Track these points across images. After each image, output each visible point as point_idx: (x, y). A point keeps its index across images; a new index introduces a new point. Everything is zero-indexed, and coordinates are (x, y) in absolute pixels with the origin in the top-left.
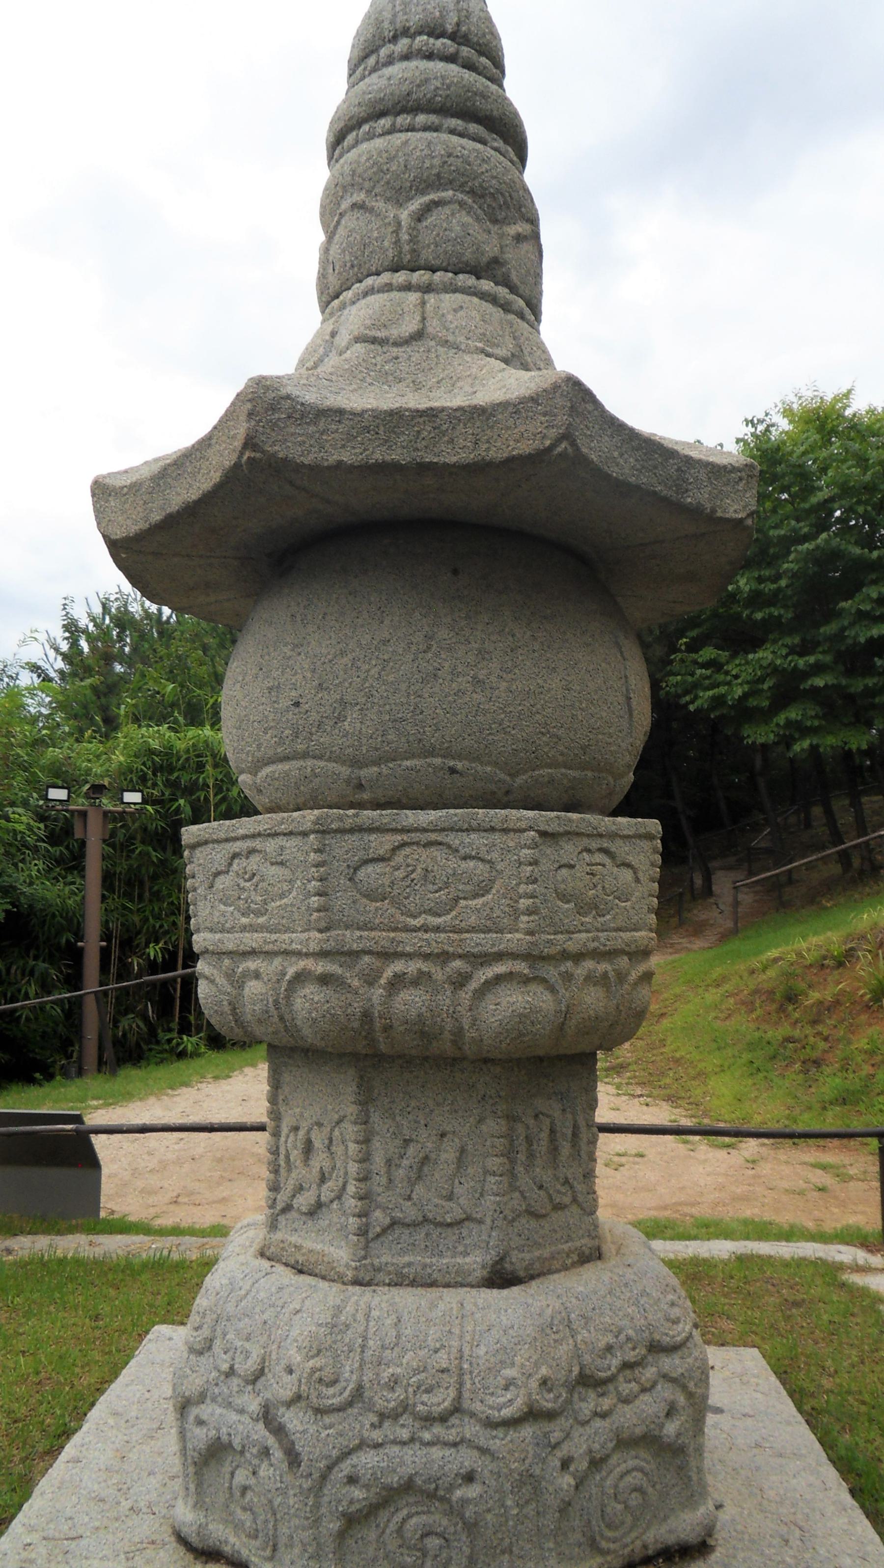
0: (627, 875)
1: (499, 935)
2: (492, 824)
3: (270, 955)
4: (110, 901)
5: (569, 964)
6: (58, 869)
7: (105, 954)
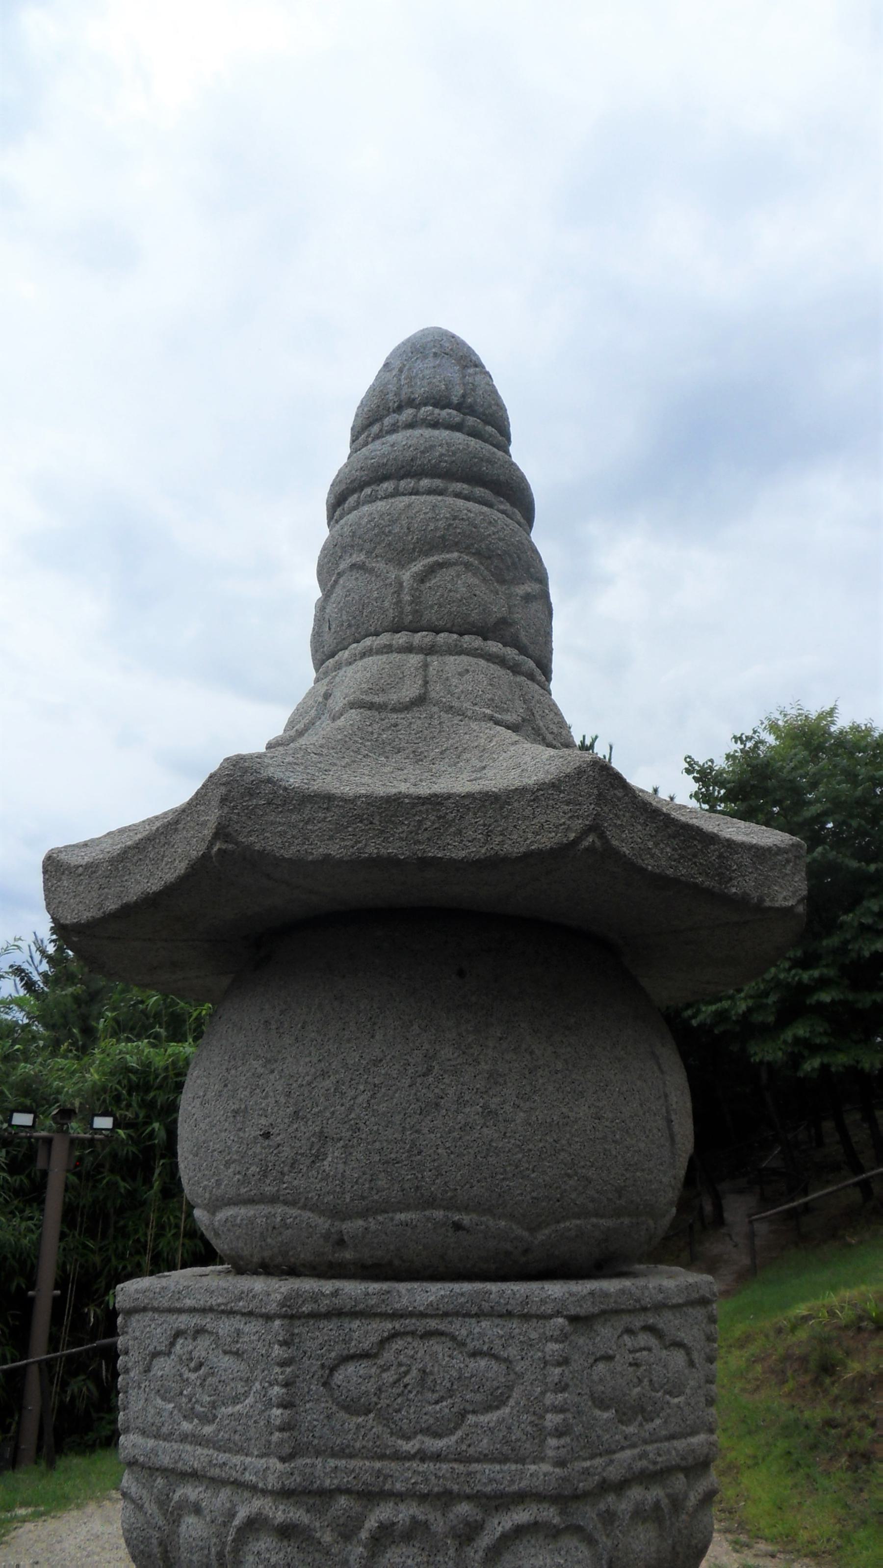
0: (678, 1358)
1: (520, 1466)
2: (509, 1308)
3: (216, 1483)
4: (70, 1239)
5: (611, 1498)
6: (16, 1202)
7: (58, 1304)
